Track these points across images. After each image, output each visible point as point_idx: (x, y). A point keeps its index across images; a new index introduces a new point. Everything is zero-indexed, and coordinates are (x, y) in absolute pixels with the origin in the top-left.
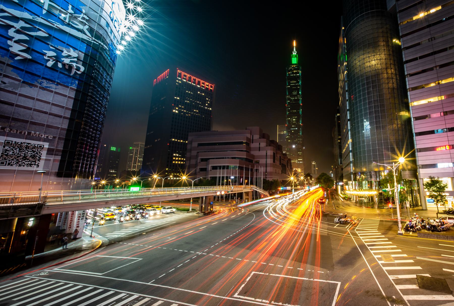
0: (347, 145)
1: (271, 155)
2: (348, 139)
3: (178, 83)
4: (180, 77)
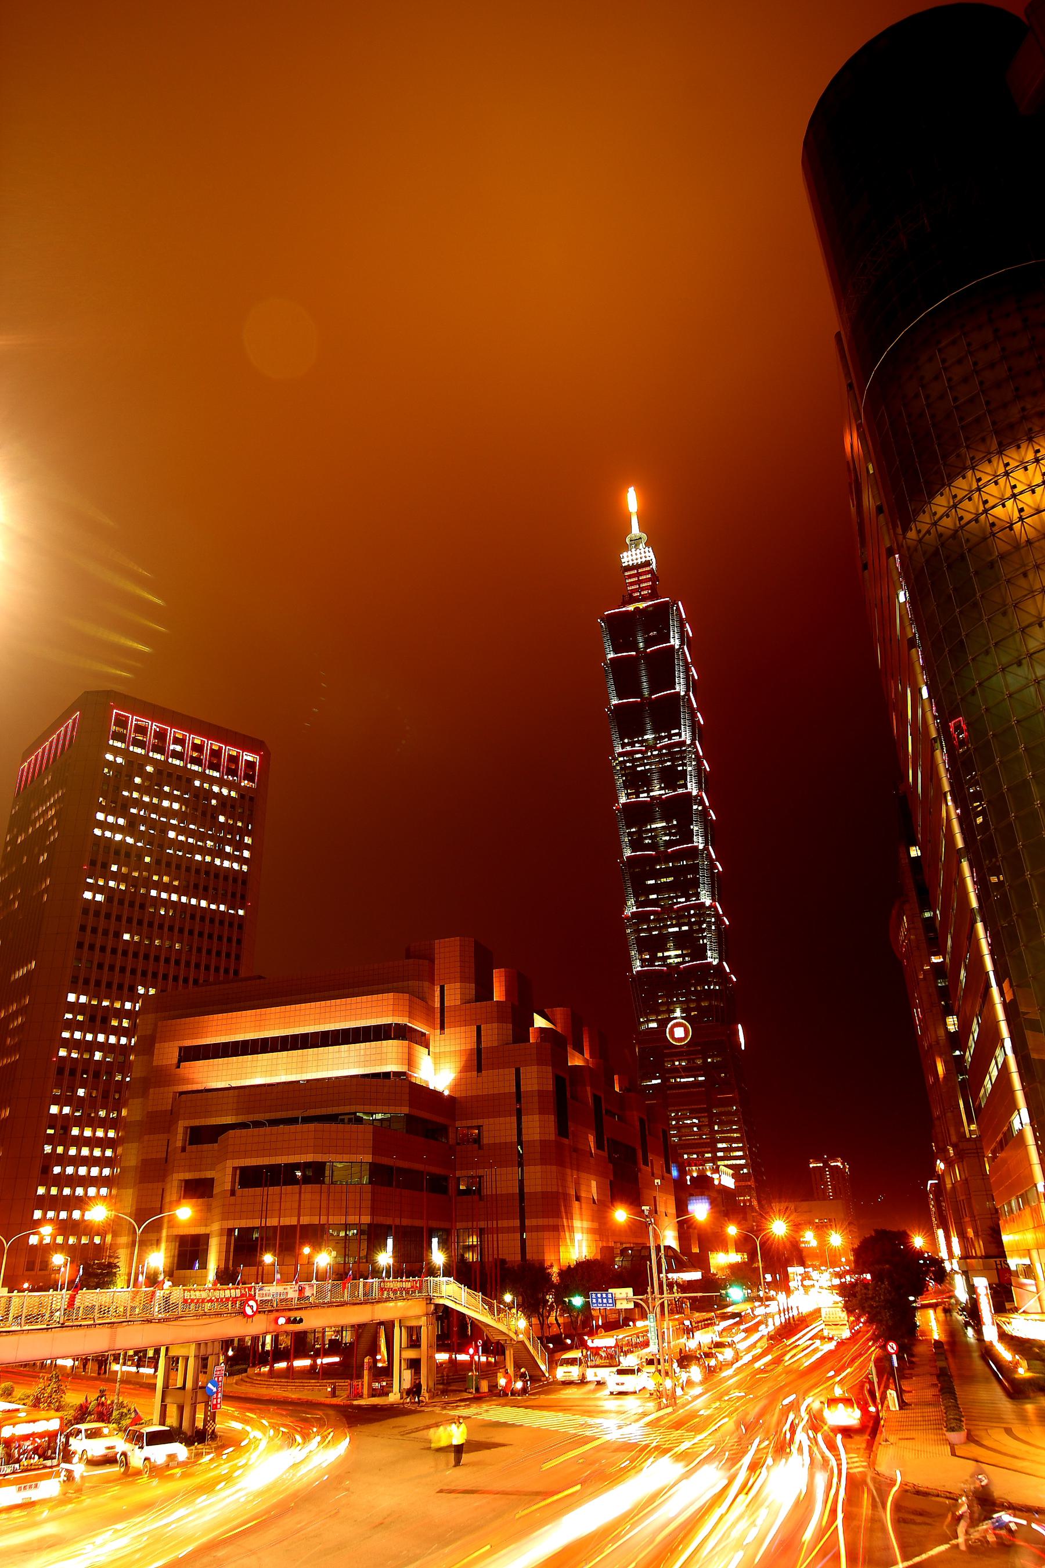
0: (994, 1072)
1: (541, 1093)
2: (1014, 1107)
3: (111, 765)
4: (120, 737)
